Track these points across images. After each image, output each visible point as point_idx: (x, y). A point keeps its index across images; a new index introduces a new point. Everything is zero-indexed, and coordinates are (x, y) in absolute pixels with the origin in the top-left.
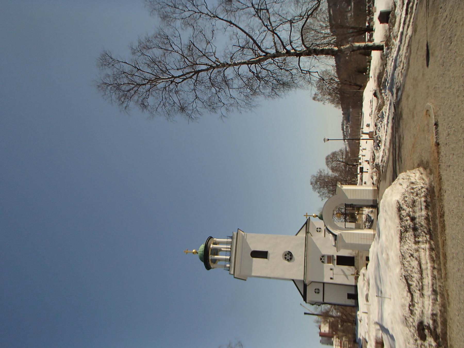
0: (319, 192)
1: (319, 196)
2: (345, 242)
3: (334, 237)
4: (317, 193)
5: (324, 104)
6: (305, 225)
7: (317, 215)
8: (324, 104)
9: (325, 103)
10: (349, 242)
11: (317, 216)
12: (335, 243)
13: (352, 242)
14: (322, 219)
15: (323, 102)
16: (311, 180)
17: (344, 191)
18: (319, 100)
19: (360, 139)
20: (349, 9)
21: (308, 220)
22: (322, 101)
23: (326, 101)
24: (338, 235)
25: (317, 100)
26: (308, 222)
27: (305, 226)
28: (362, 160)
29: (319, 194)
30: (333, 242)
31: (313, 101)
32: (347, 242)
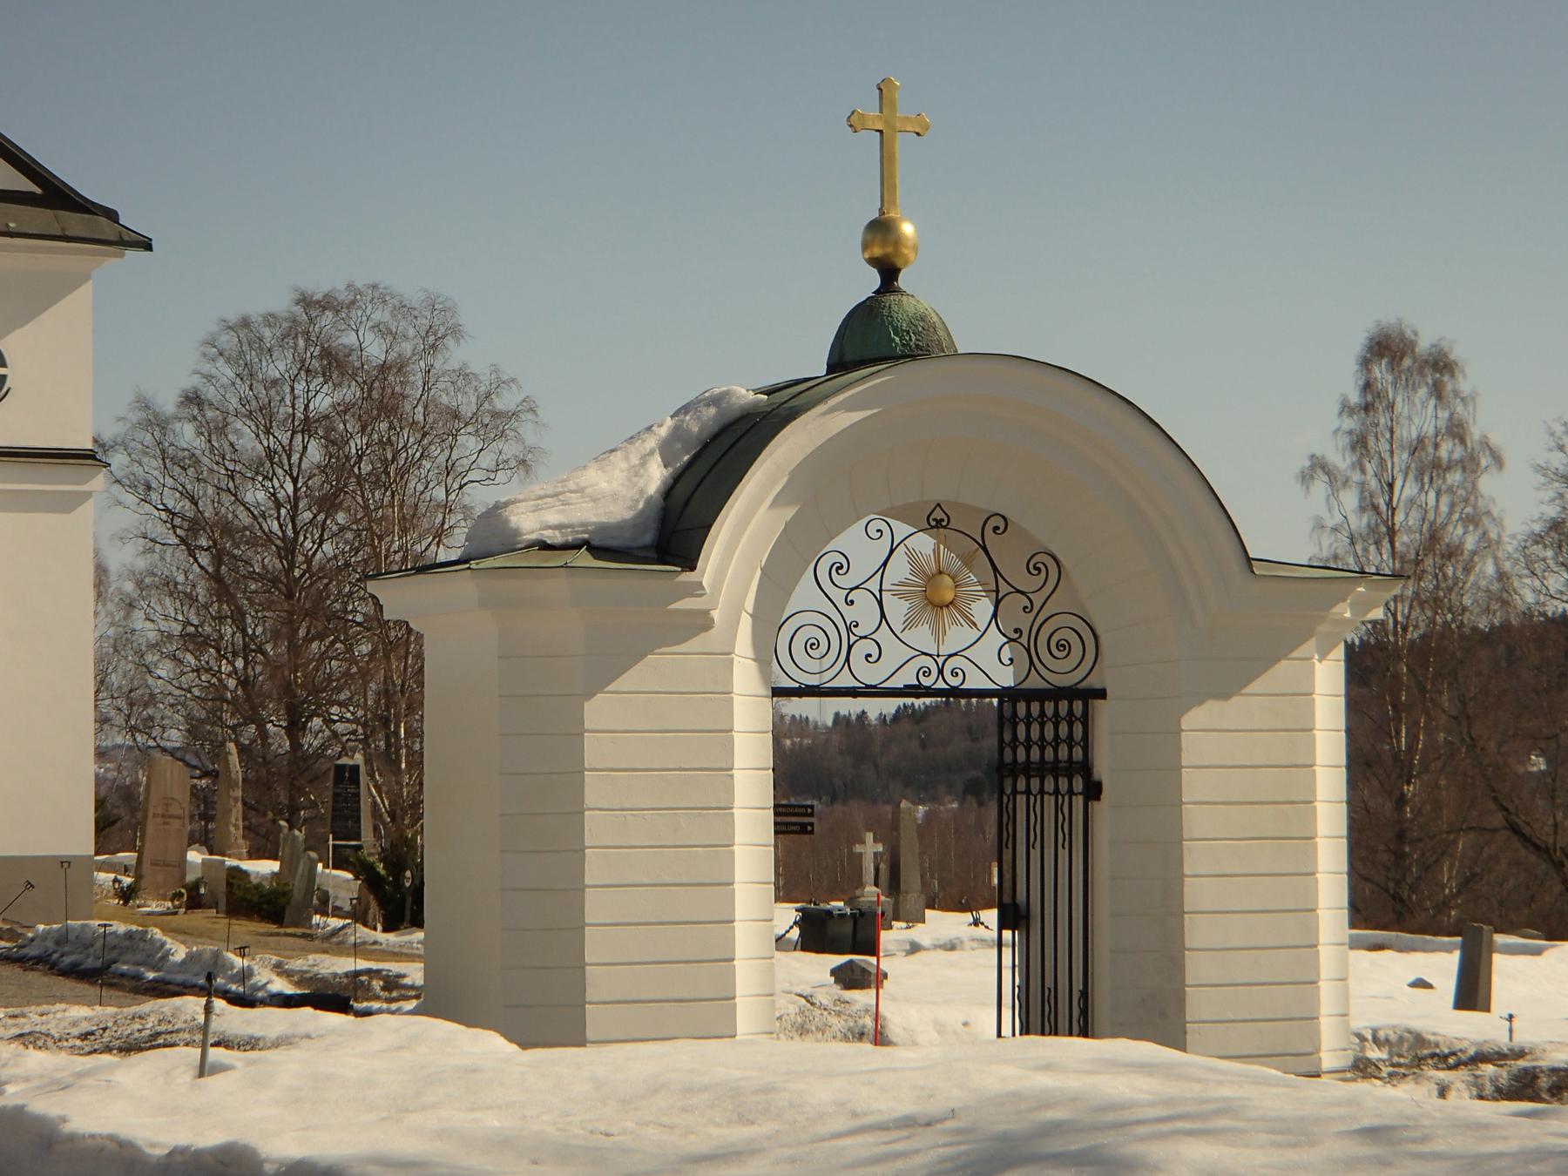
0: (193, 399)
1: (144, 404)
2: (599, 680)
3: (636, 524)
4: (191, 382)
5: (1306, 477)
6: (25, 185)
7: (903, 281)
8: (1319, 466)
9: (1320, 486)
10: (594, 749)
11: (889, 272)
12: (544, 546)
13: (595, 790)
14: (841, 363)
15: (1341, 460)
16: (380, 296)
17: (1283, 670)
18: (1371, 401)
19: (1184, 913)
20: (285, 827)
21: (104, 227)
22: (1359, 443)
23: (1350, 499)
24: (696, 589)
25: (1367, 386)
26: (75, 222)
27: (25, 185)
28: (318, 957)
29: (168, 403)
30: (553, 517)
31: (1356, 344)
32: (598, 711)
